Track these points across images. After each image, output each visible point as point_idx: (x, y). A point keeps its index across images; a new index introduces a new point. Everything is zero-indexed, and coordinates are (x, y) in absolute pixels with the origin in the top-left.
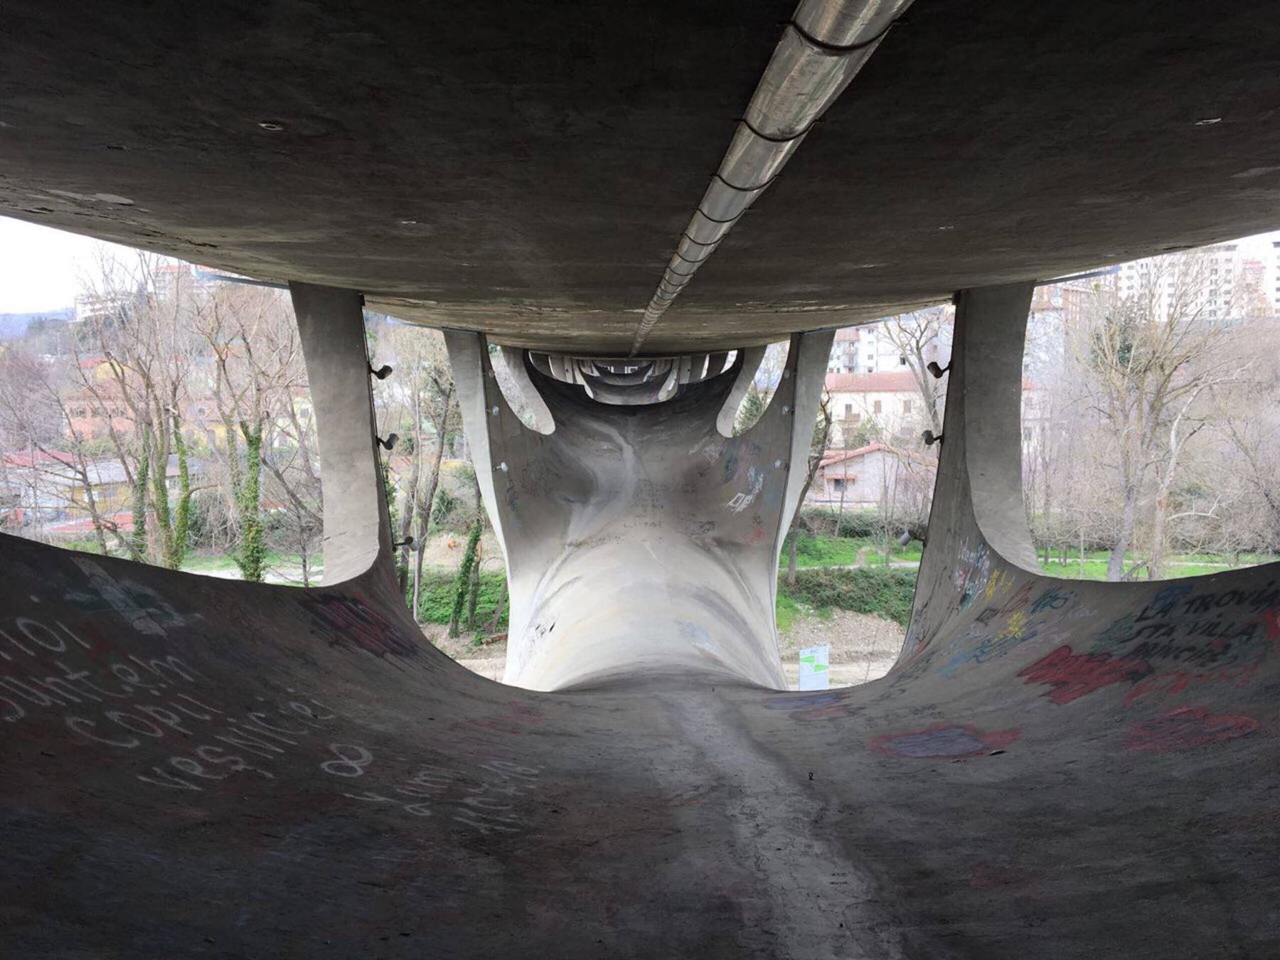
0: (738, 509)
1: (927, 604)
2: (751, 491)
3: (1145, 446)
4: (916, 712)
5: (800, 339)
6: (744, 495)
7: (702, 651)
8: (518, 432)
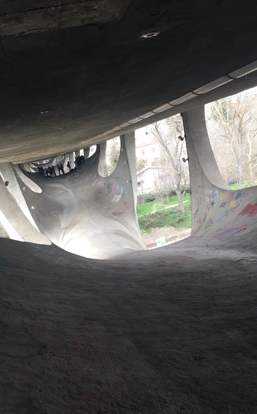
0: (117, 201)
1: (197, 211)
2: (120, 193)
4: (218, 231)
5: (124, 136)
6: (117, 196)
8: (32, 195)
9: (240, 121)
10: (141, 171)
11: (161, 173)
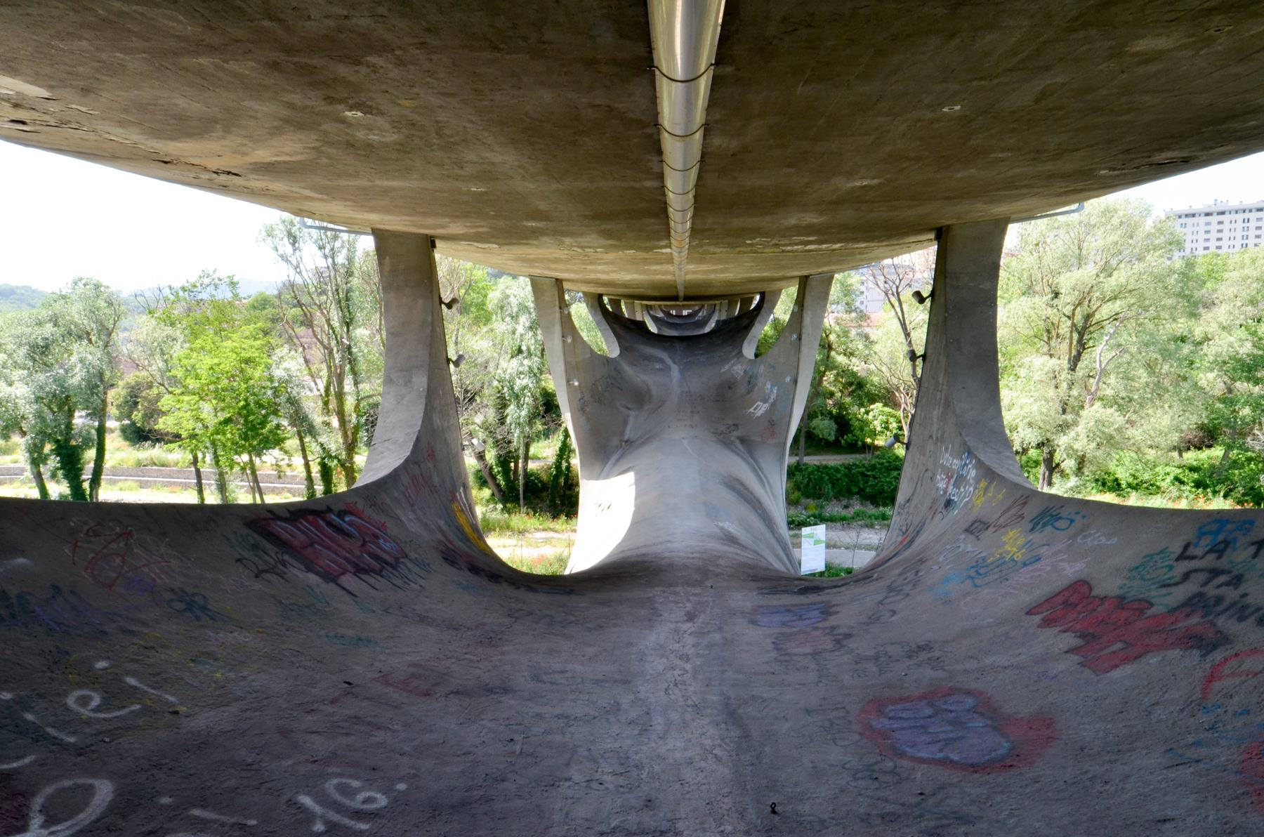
0: (757, 415)
1: (909, 500)
7: (722, 529)
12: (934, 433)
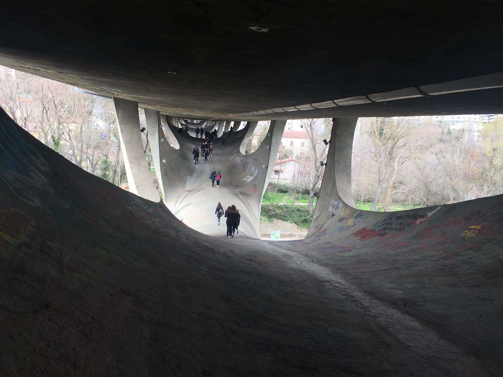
0: (248, 181)
1: (318, 217)
3: (386, 166)
4: (325, 244)
5: (275, 122)
9: (393, 144)
10: (284, 160)
11: (302, 169)
12: (329, 193)
